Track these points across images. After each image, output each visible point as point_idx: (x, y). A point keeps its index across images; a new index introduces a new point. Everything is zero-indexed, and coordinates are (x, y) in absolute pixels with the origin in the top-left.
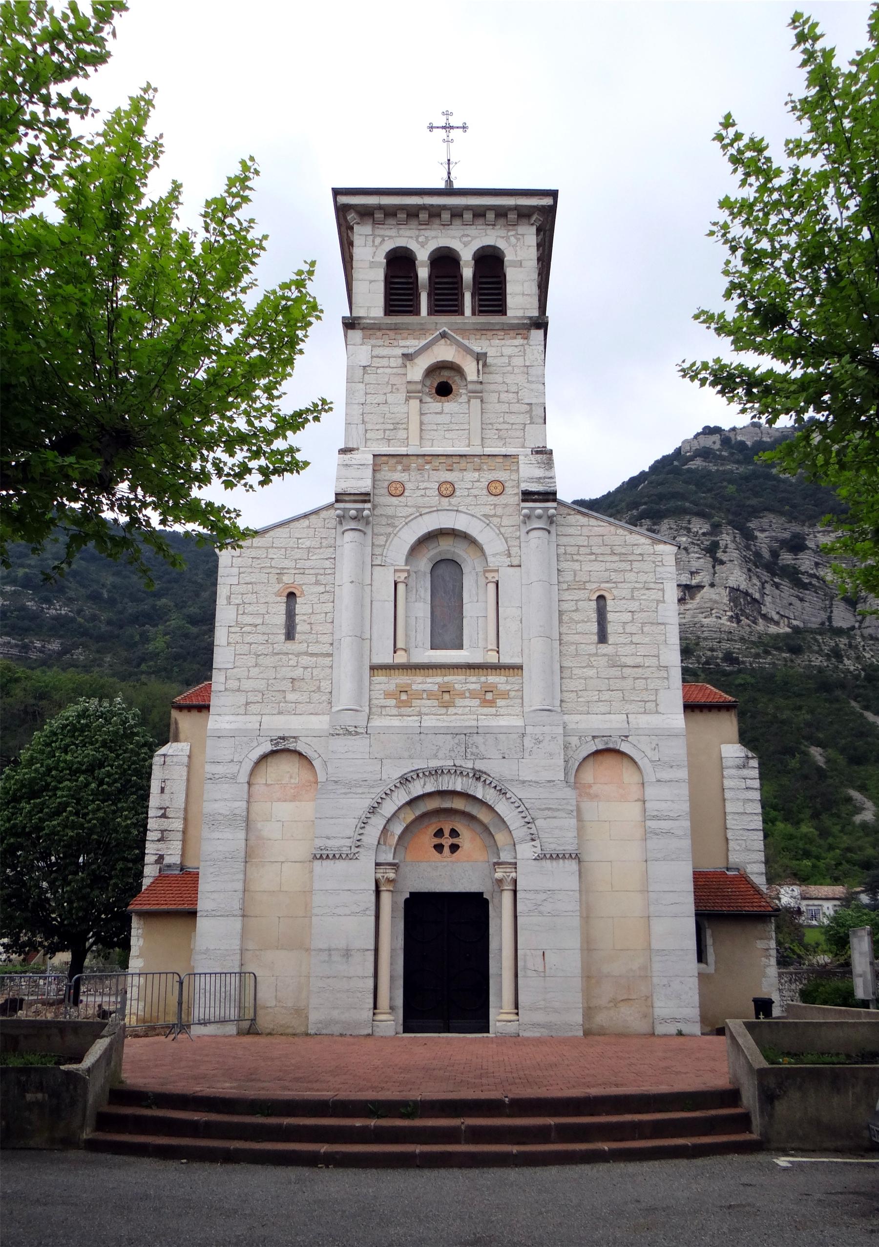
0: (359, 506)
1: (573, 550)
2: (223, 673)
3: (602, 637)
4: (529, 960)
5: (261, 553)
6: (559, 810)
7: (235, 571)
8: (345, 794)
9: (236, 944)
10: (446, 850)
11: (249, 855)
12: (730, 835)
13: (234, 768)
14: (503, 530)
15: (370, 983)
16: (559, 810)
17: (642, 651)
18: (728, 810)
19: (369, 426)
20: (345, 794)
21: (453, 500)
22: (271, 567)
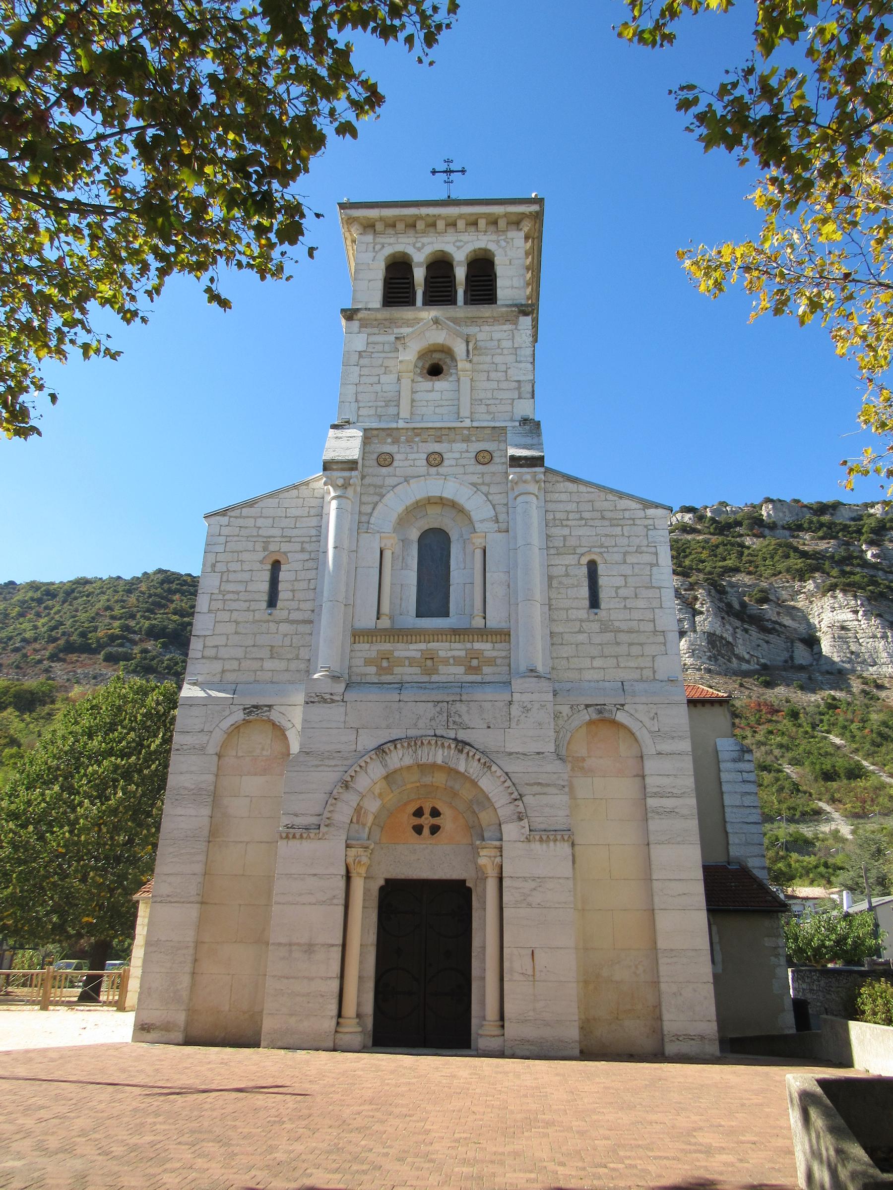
0: (346, 474)
1: (562, 516)
2: (201, 640)
3: (594, 602)
4: (516, 962)
5: (251, 522)
6: (548, 785)
7: (222, 539)
8: (317, 766)
9: (190, 936)
10: (426, 831)
11: (214, 834)
12: (729, 829)
13: (204, 738)
14: (490, 497)
15: (335, 985)
16: (548, 785)
17: (636, 615)
18: (726, 803)
19: (361, 405)
20: (317, 766)
21: (441, 470)
22: (258, 536)
